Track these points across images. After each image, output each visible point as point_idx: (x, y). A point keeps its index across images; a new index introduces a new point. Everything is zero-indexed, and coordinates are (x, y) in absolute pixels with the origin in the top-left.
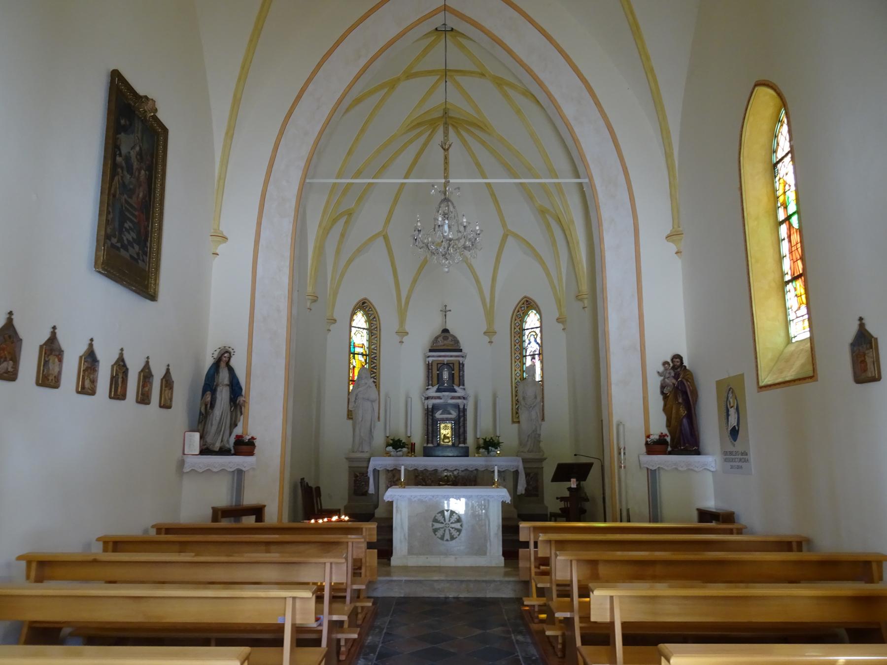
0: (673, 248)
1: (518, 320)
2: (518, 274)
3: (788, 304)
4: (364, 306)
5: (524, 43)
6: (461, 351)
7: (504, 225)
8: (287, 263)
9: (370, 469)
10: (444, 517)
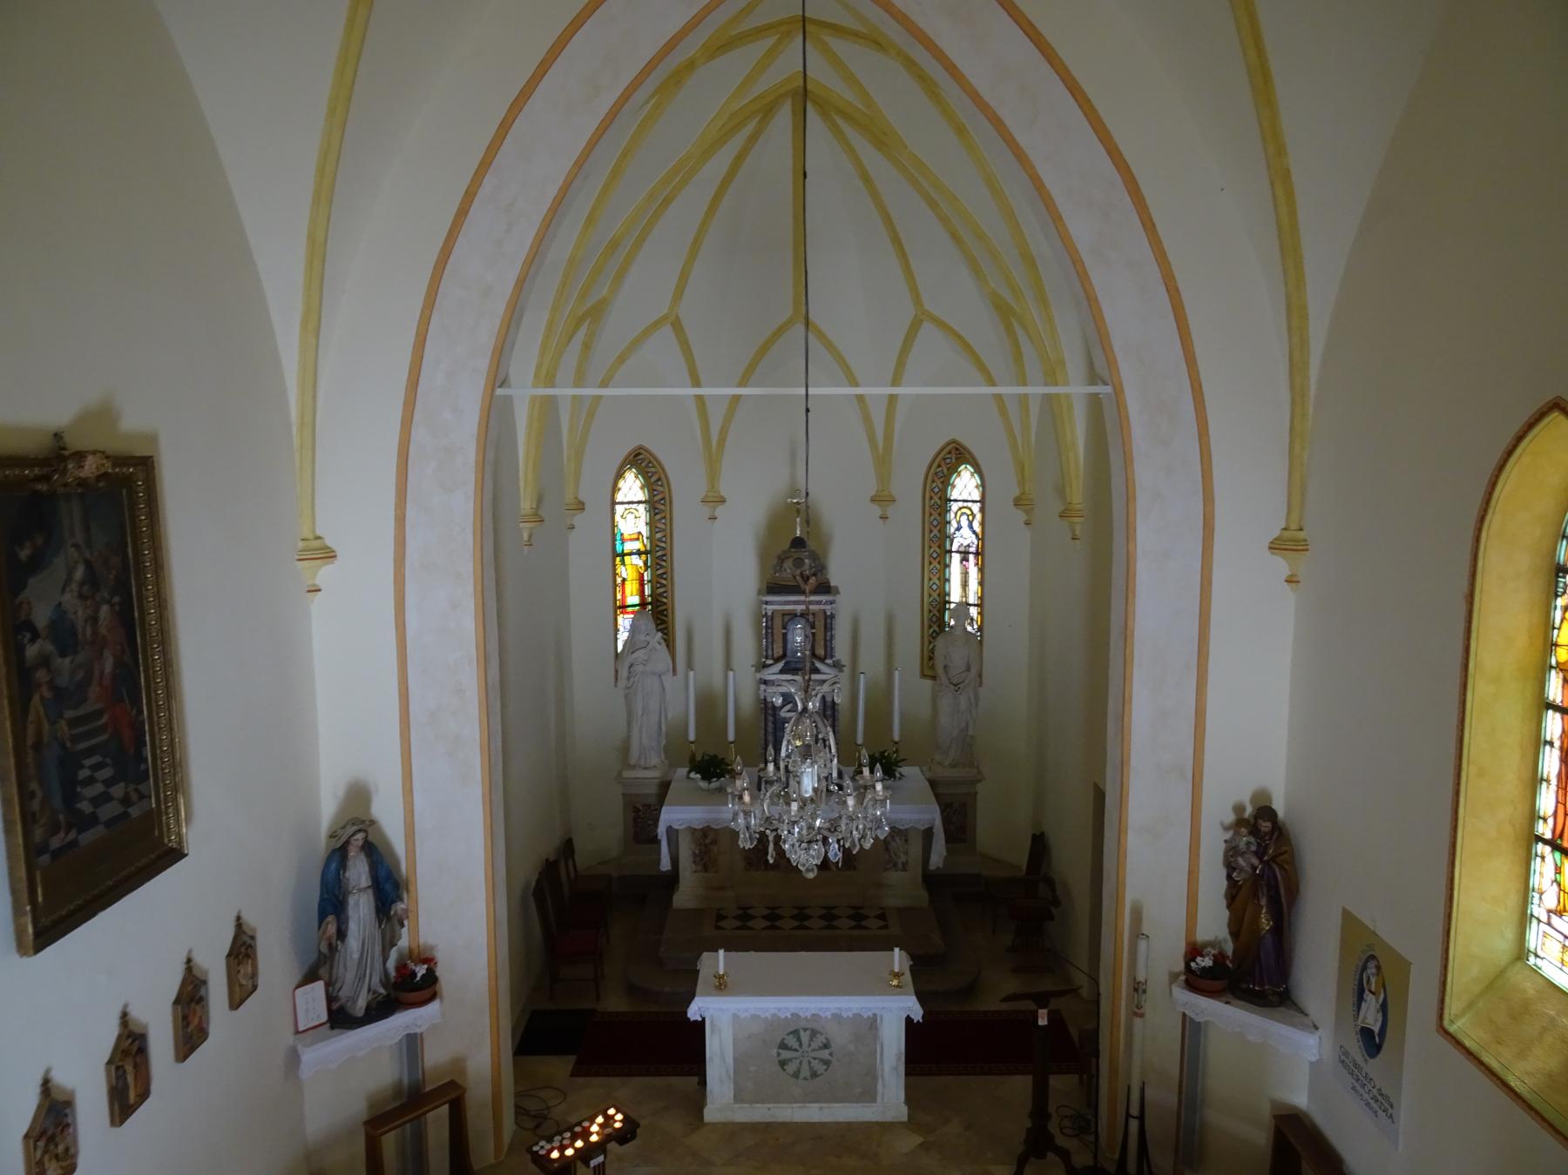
0: (1280, 566)
1: (938, 483)
2: (939, 392)
3: (1535, 881)
4: (640, 460)
5: (990, 56)
6: (825, 588)
7: (917, 300)
8: (470, 589)
9: (661, 830)
10: (799, 1039)
